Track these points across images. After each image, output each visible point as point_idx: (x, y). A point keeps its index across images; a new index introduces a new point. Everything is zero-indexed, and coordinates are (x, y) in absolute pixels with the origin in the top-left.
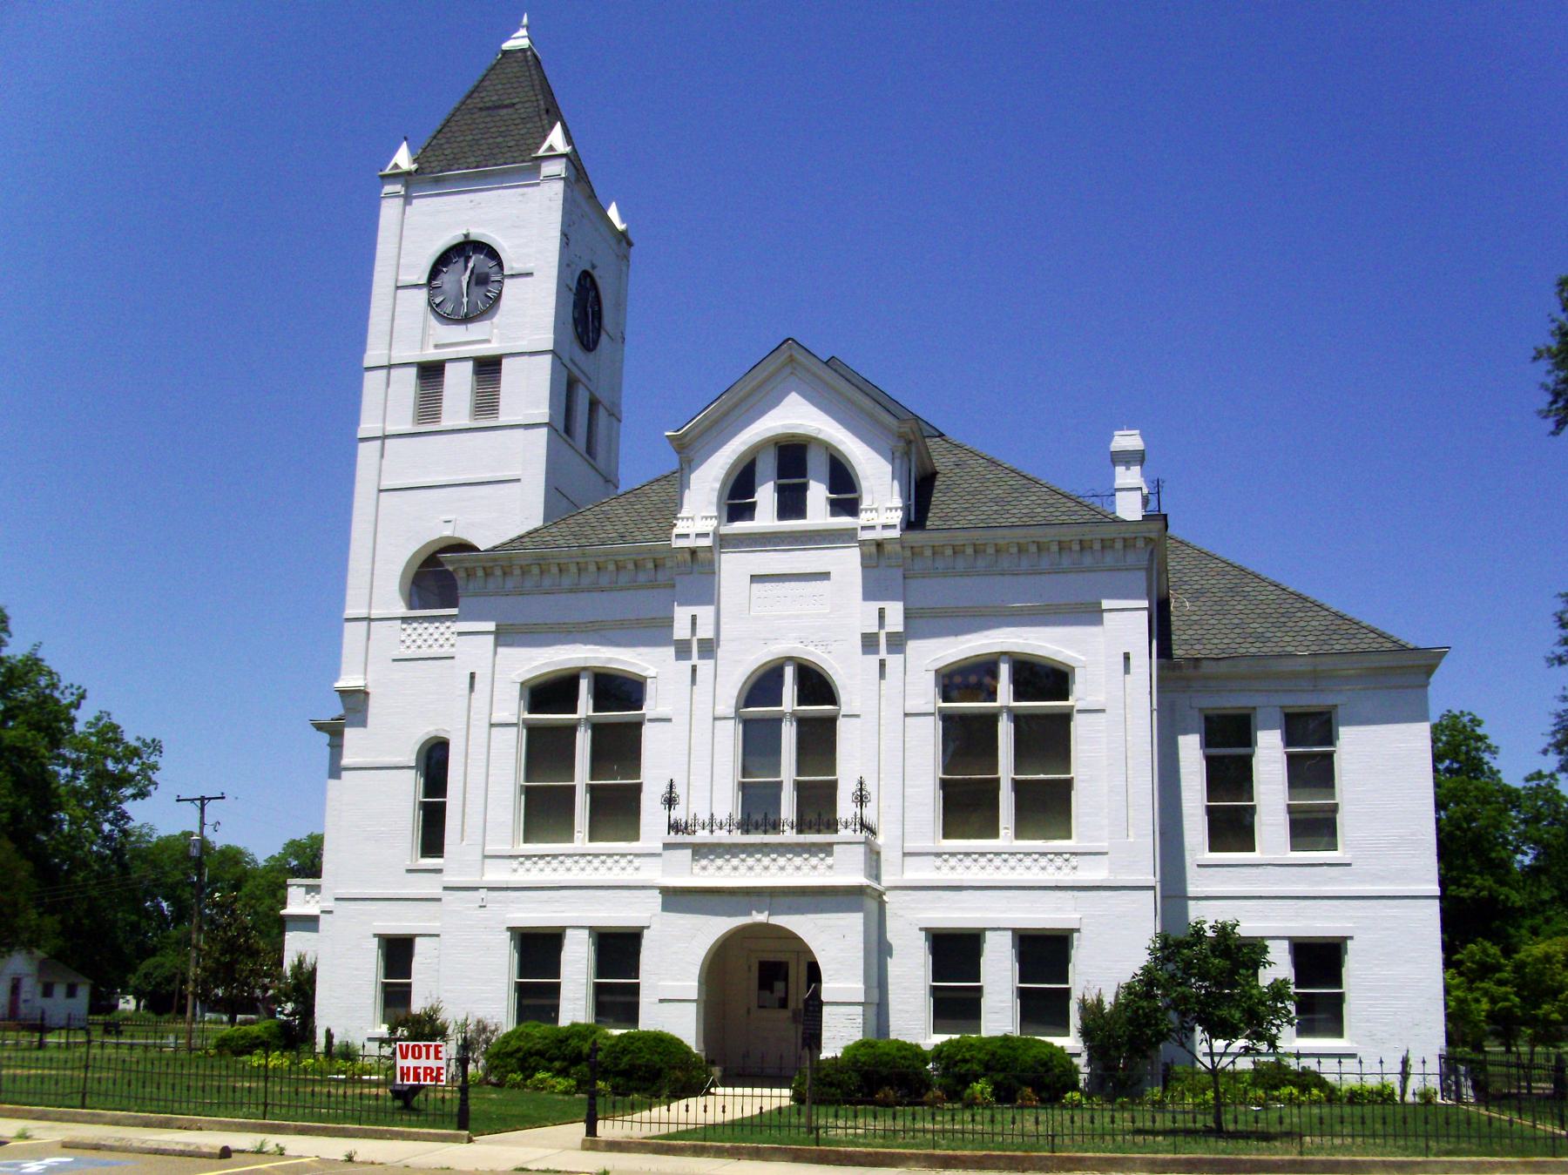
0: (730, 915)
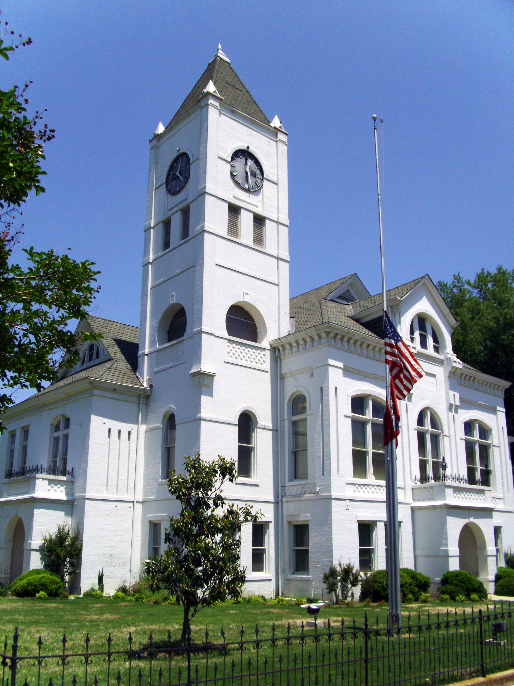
0: (464, 518)
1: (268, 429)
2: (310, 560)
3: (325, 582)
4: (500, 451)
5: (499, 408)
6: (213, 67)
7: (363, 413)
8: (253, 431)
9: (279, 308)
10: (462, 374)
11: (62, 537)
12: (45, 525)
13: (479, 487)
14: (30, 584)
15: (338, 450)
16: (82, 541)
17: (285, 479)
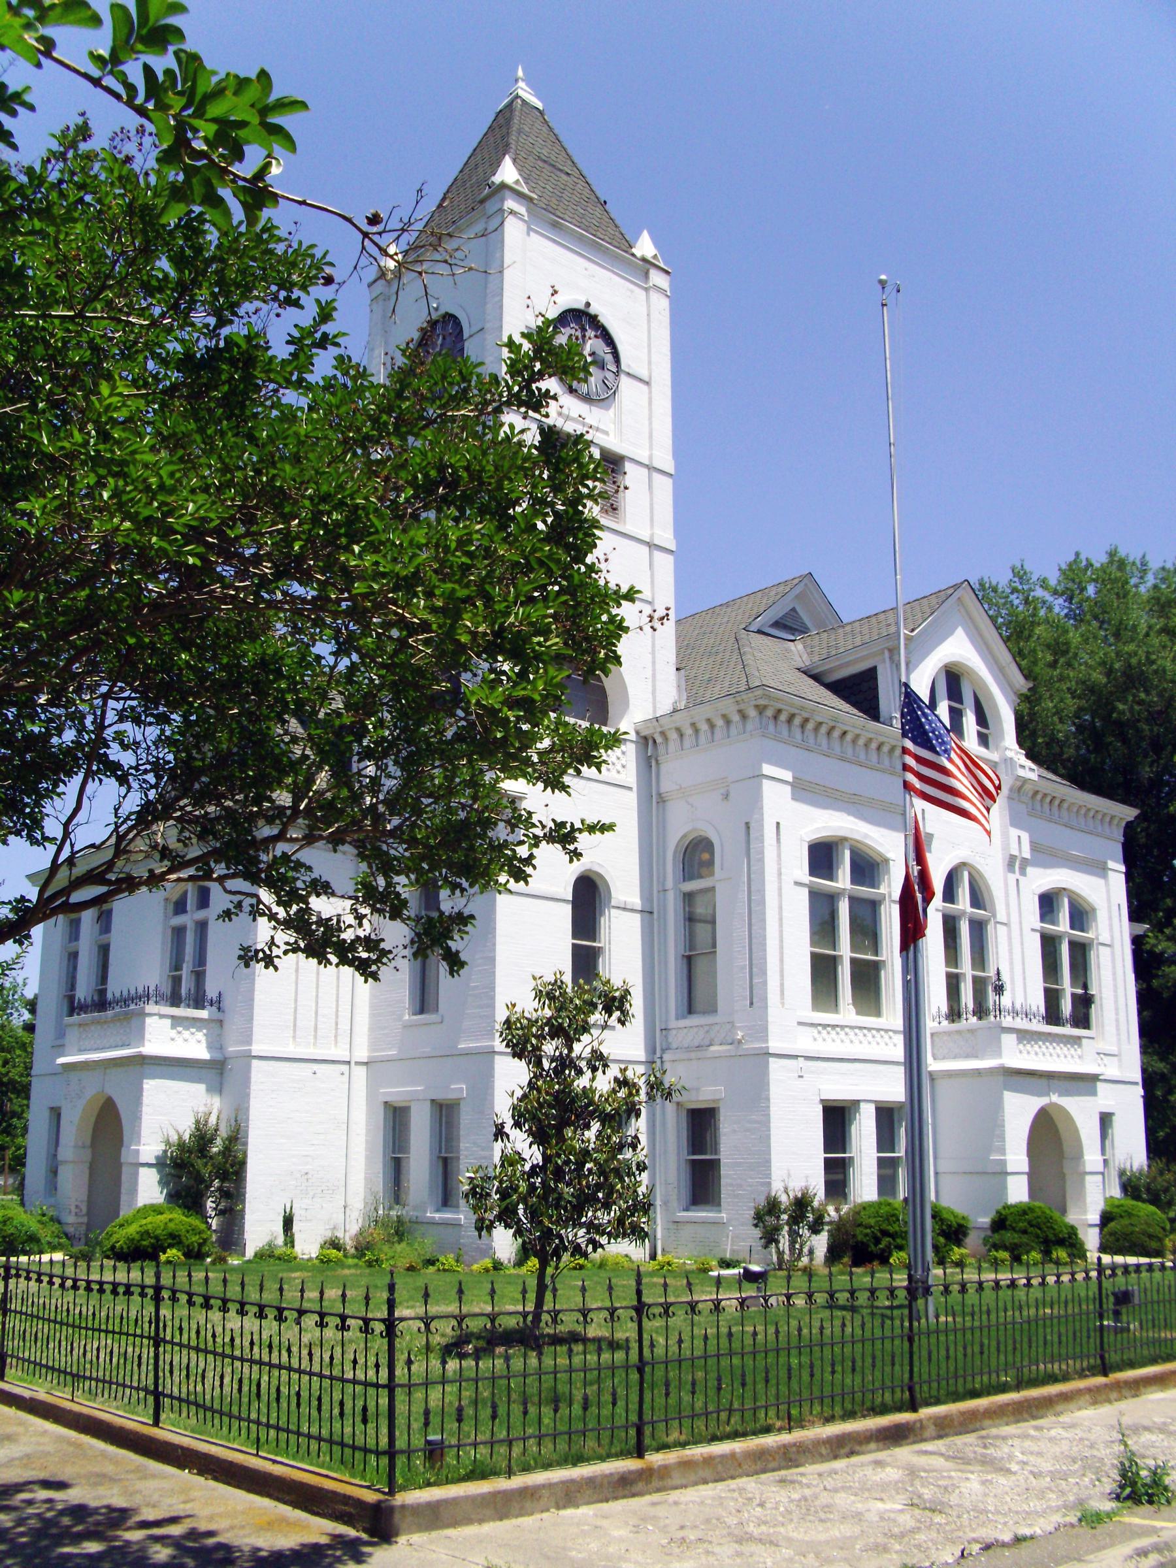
1: (632, 910)
2: (723, 1182)
3: (756, 1226)
4: (1113, 954)
5: (1111, 864)
6: (509, 121)
7: (830, 876)
8: (602, 914)
9: (653, 653)
10: (1036, 792)
11: (203, 1137)
12: (166, 1115)
13: (1068, 1030)
14: (145, 1234)
15: (782, 954)
16: (246, 1144)
17: (667, 1012)
